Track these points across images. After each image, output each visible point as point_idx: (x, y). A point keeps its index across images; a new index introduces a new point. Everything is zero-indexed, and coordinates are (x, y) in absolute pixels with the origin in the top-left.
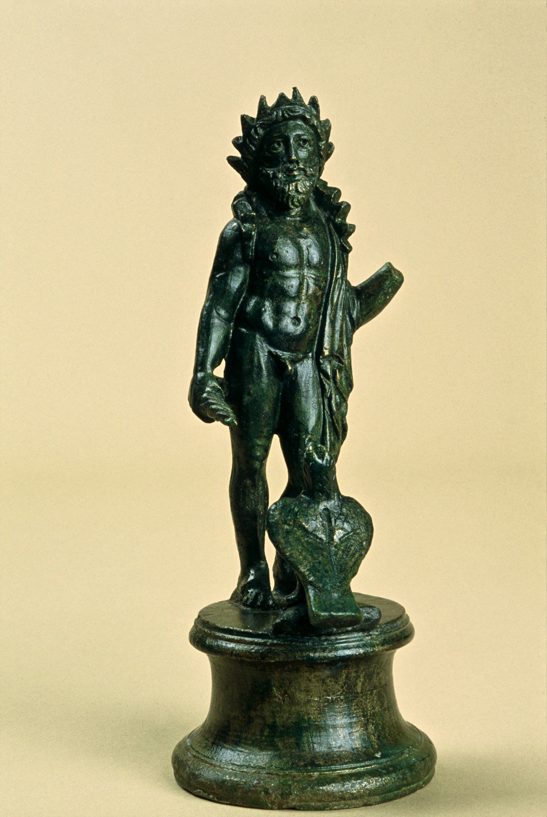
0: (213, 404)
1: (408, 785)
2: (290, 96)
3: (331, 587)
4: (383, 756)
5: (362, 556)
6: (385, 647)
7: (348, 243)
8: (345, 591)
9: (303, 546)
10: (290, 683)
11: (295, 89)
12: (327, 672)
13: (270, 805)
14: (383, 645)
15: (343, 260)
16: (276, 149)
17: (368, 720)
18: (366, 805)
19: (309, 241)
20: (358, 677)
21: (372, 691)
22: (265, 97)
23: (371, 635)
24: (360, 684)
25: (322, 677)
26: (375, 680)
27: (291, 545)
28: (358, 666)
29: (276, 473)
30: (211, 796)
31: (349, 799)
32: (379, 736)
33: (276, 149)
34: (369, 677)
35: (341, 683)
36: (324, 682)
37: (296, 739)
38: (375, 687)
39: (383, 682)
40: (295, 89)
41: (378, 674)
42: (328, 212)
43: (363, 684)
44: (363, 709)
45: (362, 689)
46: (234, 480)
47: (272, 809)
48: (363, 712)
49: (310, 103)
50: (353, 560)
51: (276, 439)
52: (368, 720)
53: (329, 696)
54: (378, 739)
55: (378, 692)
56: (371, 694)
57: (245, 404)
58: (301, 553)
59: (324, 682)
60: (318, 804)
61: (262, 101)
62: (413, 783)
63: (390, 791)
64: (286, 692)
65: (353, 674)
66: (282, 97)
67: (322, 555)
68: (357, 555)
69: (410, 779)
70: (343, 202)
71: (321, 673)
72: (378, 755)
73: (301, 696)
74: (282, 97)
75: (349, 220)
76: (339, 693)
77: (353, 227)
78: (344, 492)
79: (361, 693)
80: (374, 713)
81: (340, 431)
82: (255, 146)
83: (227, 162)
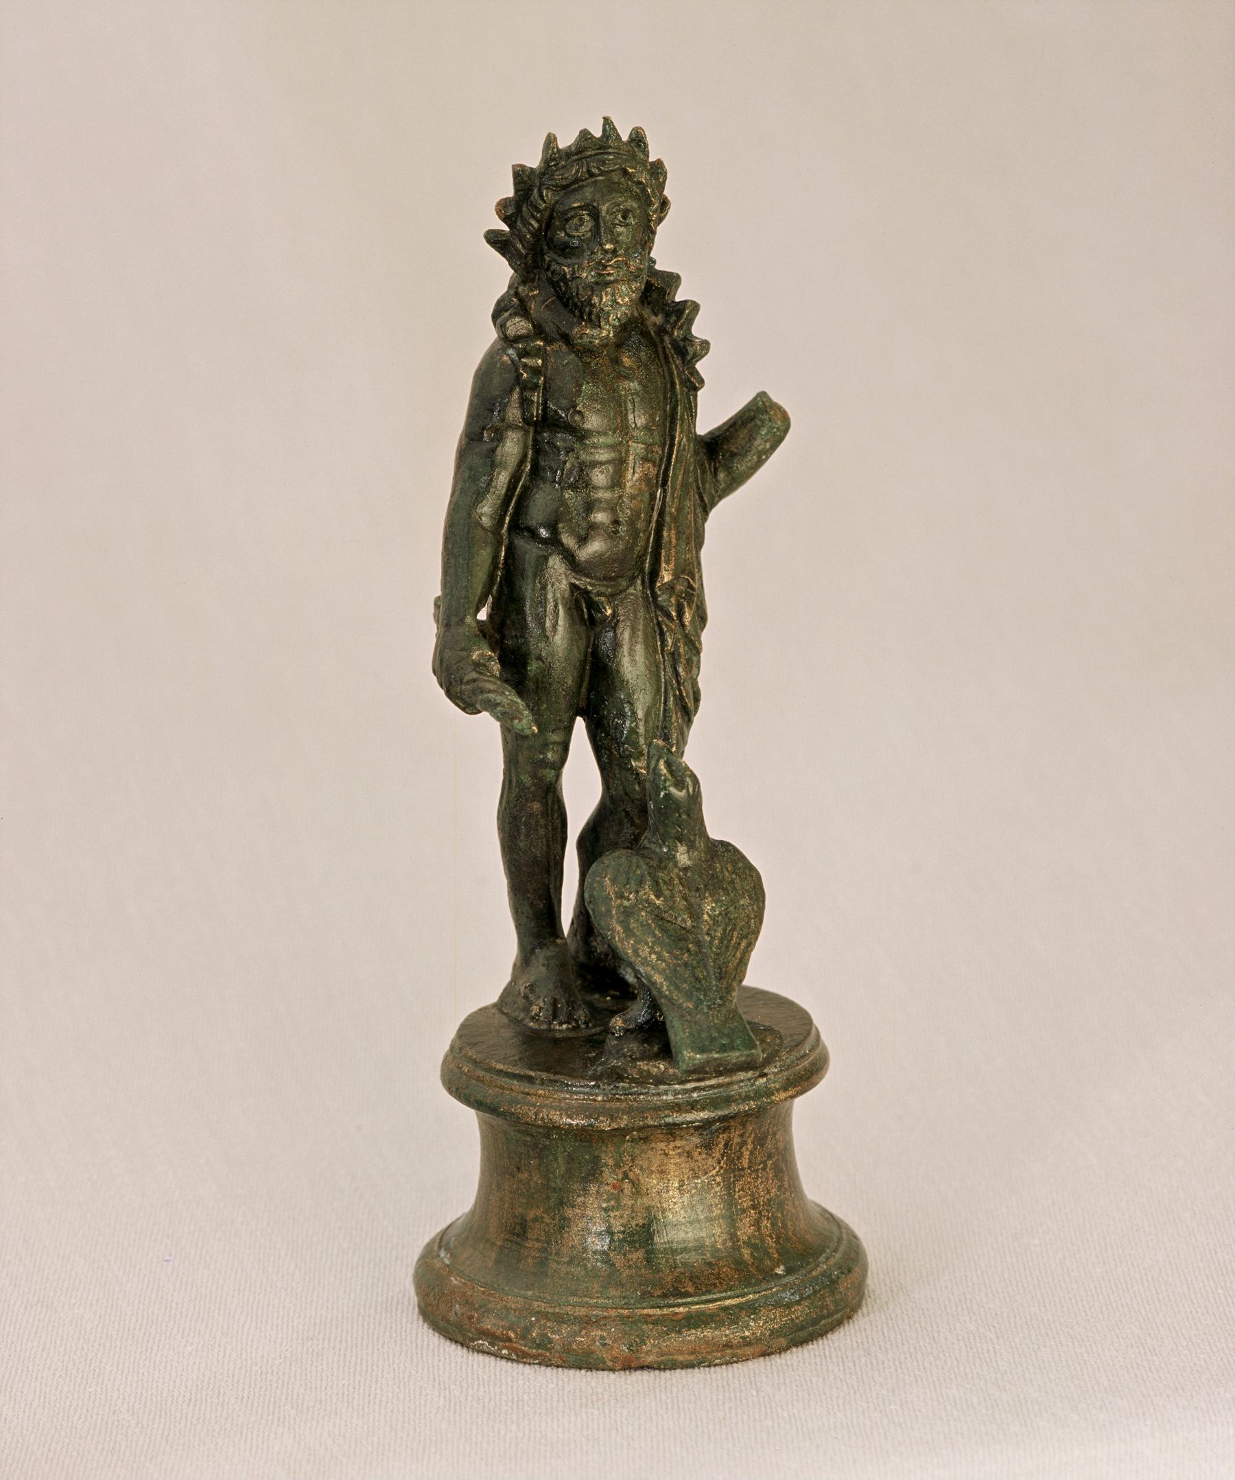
0: (490, 691)
1: (830, 1315)
2: (597, 133)
3: (709, 1007)
4: (789, 1271)
5: (750, 945)
6: (790, 1093)
7: (695, 373)
8: (729, 1012)
9: (655, 935)
10: (633, 1160)
11: (607, 121)
12: (696, 1140)
13: (610, 1364)
14: (785, 1089)
15: (690, 402)
16: (575, 225)
17: (760, 1213)
18: (764, 1354)
19: (634, 385)
20: (744, 1143)
21: (764, 1162)
22: (555, 139)
23: (765, 1075)
24: (746, 1154)
25: (687, 1148)
26: (769, 1144)
27: (634, 935)
28: (744, 1125)
29: (582, 787)
30: (504, 1352)
31: (739, 1347)
32: (778, 1238)
33: (575, 225)
34: (761, 1141)
35: (717, 1155)
36: (689, 1155)
37: (647, 1252)
38: (770, 1156)
39: (781, 1145)
40: (607, 121)
41: (774, 1134)
42: (660, 316)
43: (752, 1153)
44: (752, 1195)
45: (750, 1162)
46: (508, 802)
47: (612, 1370)
48: (753, 1200)
49: (631, 140)
50: (738, 955)
51: (580, 723)
52: (760, 1213)
53: (698, 1178)
54: (777, 1242)
55: (774, 1163)
56: (764, 1169)
57: (531, 674)
58: (652, 951)
59: (689, 1155)
60: (692, 1357)
61: (550, 140)
62: (837, 1312)
63: (802, 1328)
64: (626, 1176)
65: (737, 1140)
66: (585, 134)
67: (688, 950)
68: (743, 944)
69: (832, 1307)
70: (686, 302)
71: (684, 1142)
72: (780, 1271)
73: (653, 1182)
74: (585, 134)
75: (698, 330)
76: (714, 1172)
77: (705, 345)
78: (715, 832)
79: (749, 1168)
80: (769, 1200)
81: (690, 705)
82: (538, 221)
83: (484, 241)
